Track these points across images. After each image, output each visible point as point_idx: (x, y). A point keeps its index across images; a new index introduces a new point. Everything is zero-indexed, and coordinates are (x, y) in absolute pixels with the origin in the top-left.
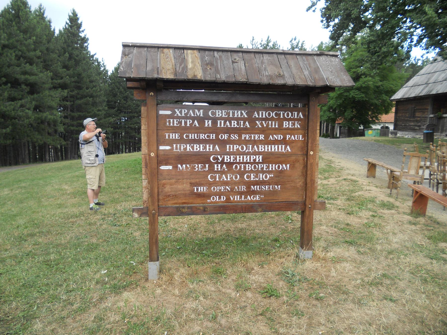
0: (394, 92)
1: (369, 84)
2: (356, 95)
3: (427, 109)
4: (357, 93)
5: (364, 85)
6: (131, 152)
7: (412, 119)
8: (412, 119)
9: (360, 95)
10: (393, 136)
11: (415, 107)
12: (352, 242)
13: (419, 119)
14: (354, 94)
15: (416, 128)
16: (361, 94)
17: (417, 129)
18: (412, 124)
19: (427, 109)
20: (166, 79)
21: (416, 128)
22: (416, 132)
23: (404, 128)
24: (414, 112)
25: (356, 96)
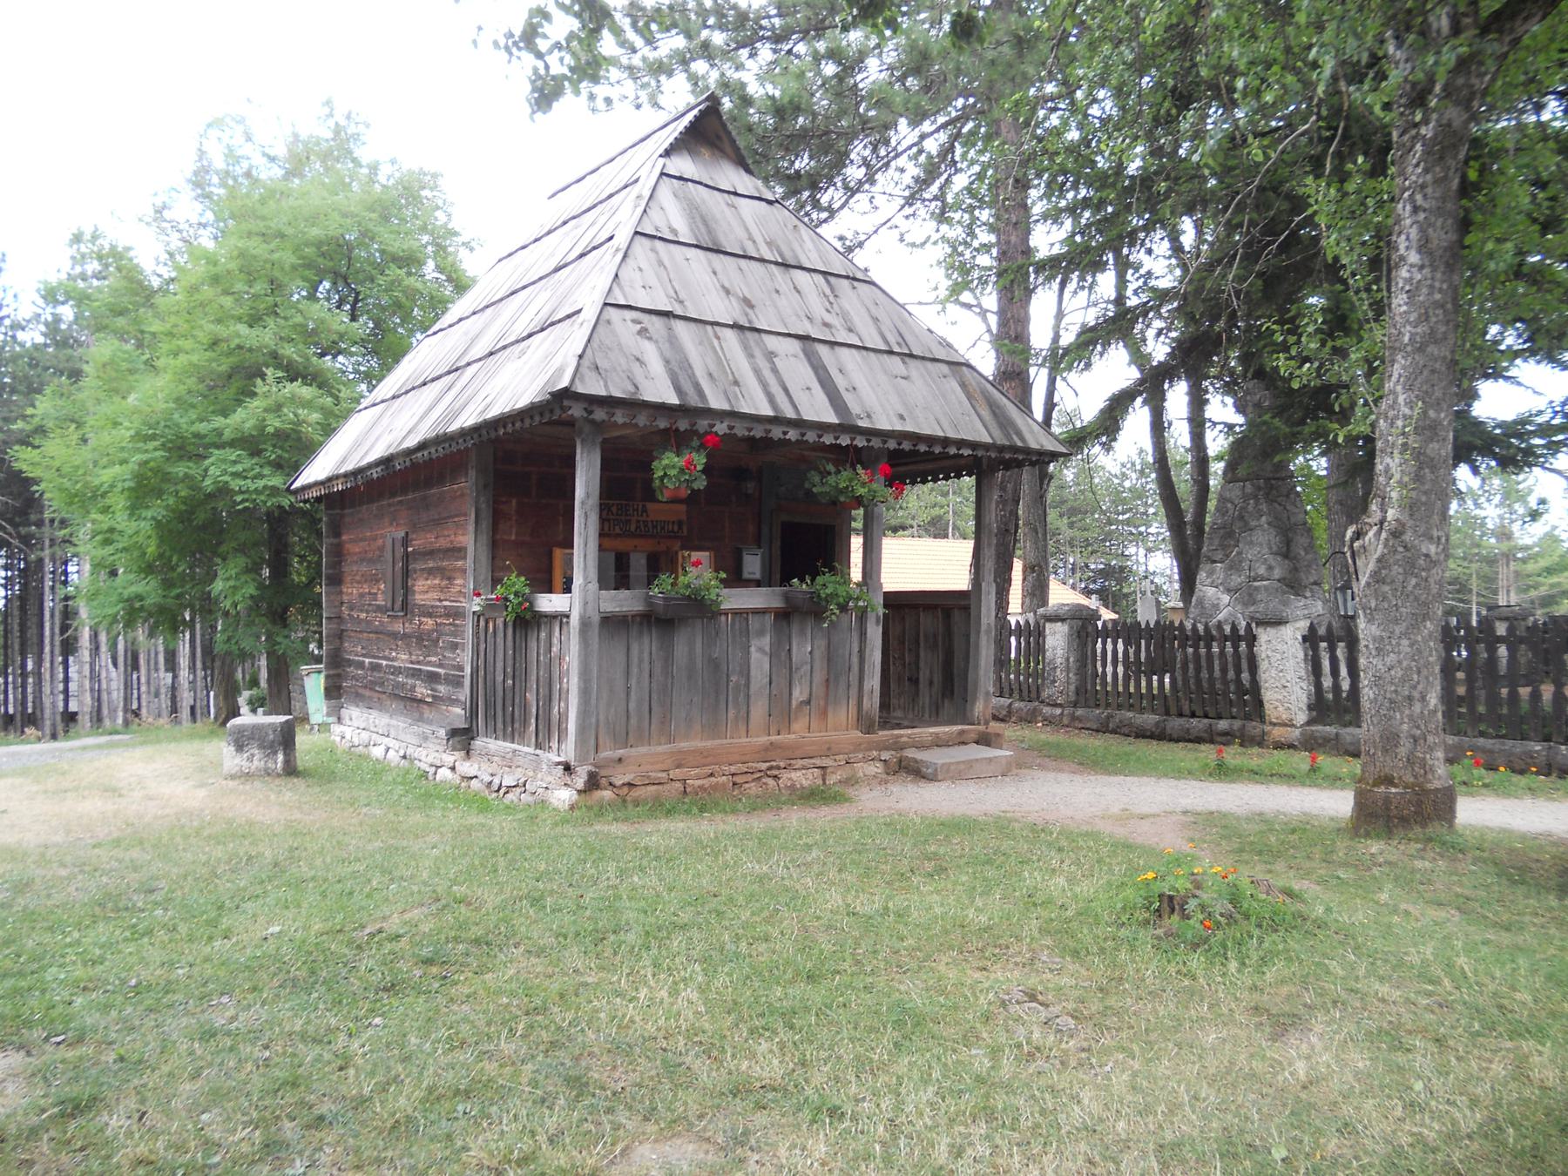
0: (306, 450)
1: (299, 423)
2: (235, 475)
3: (459, 552)
4: (239, 468)
5: (273, 424)
6: (946, 536)
7: (398, 627)
8: (398, 627)
9: (260, 476)
10: (257, 763)
11: (406, 541)
12: (1358, 121)
13: (429, 623)
14: (225, 472)
15: (422, 690)
16: (266, 471)
17: (421, 701)
18: (402, 659)
19: (459, 552)
20: (375, 473)
21: (422, 690)
22: (421, 719)
23: (370, 686)
24: (406, 573)
25: (236, 484)
